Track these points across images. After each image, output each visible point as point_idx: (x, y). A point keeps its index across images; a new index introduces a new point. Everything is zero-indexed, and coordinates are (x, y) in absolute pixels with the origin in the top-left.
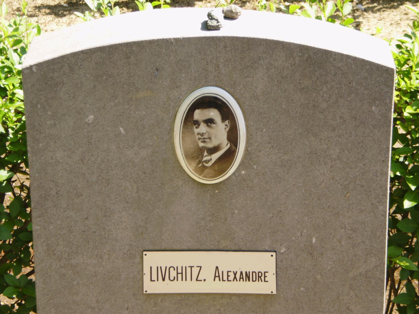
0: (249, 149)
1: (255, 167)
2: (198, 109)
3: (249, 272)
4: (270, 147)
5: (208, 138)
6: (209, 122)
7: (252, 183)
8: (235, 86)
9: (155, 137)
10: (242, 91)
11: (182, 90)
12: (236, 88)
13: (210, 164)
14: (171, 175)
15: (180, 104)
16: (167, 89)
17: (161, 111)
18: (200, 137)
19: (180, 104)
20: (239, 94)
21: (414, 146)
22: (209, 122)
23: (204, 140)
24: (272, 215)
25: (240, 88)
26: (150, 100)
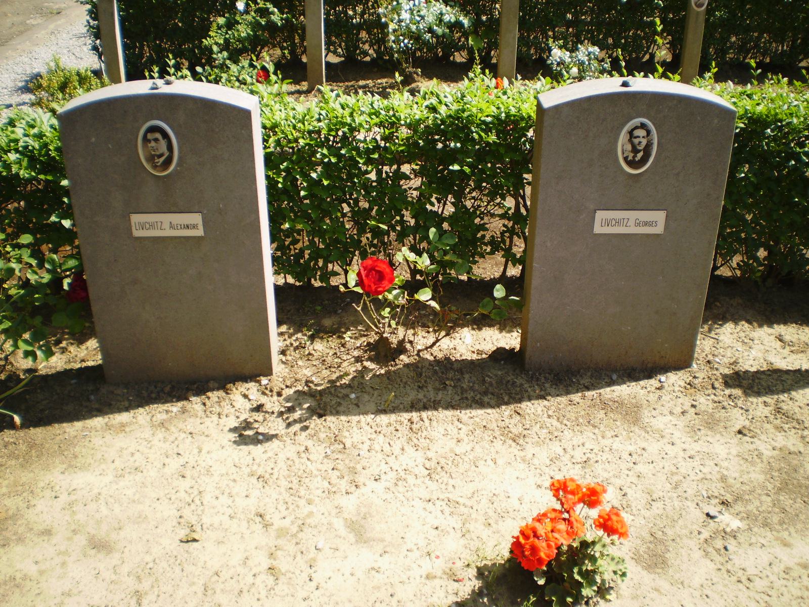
6: (156, 140)
13: (159, 164)
22: (156, 140)
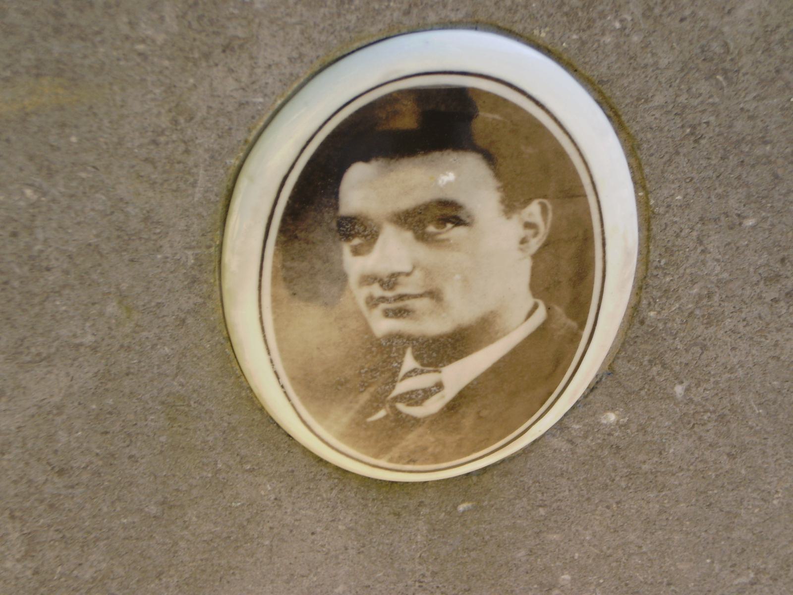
0: (652, 314)
1: (679, 390)
2: (366, 159)
4: (774, 295)
5: (421, 296)
7: (655, 459)
8: (594, 15)
9: (112, 308)
10: (635, 39)
11: (261, 62)
12: (599, 23)
13: (434, 405)
14: (216, 464)
15: (254, 133)
16: (166, 63)
17: (139, 176)
18: (377, 291)
19: (251, 138)
20: (613, 58)
23: (400, 304)
24: (752, 575)
25: (621, 21)
26: (63, 125)
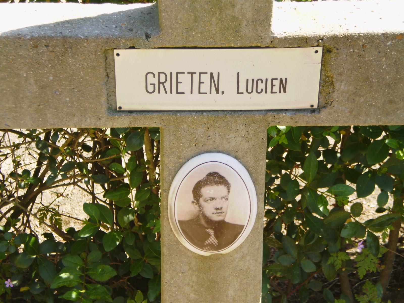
2: (27, 234)
3: (171, 73)
21: (388, 157)
